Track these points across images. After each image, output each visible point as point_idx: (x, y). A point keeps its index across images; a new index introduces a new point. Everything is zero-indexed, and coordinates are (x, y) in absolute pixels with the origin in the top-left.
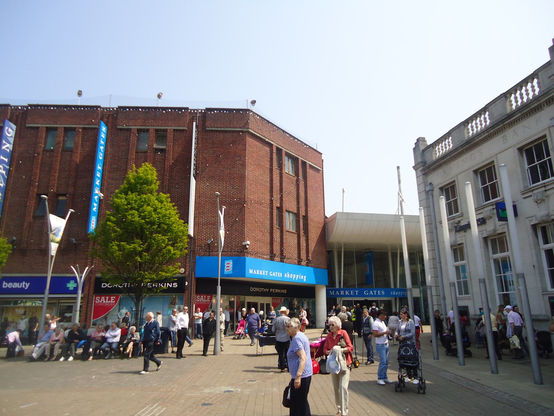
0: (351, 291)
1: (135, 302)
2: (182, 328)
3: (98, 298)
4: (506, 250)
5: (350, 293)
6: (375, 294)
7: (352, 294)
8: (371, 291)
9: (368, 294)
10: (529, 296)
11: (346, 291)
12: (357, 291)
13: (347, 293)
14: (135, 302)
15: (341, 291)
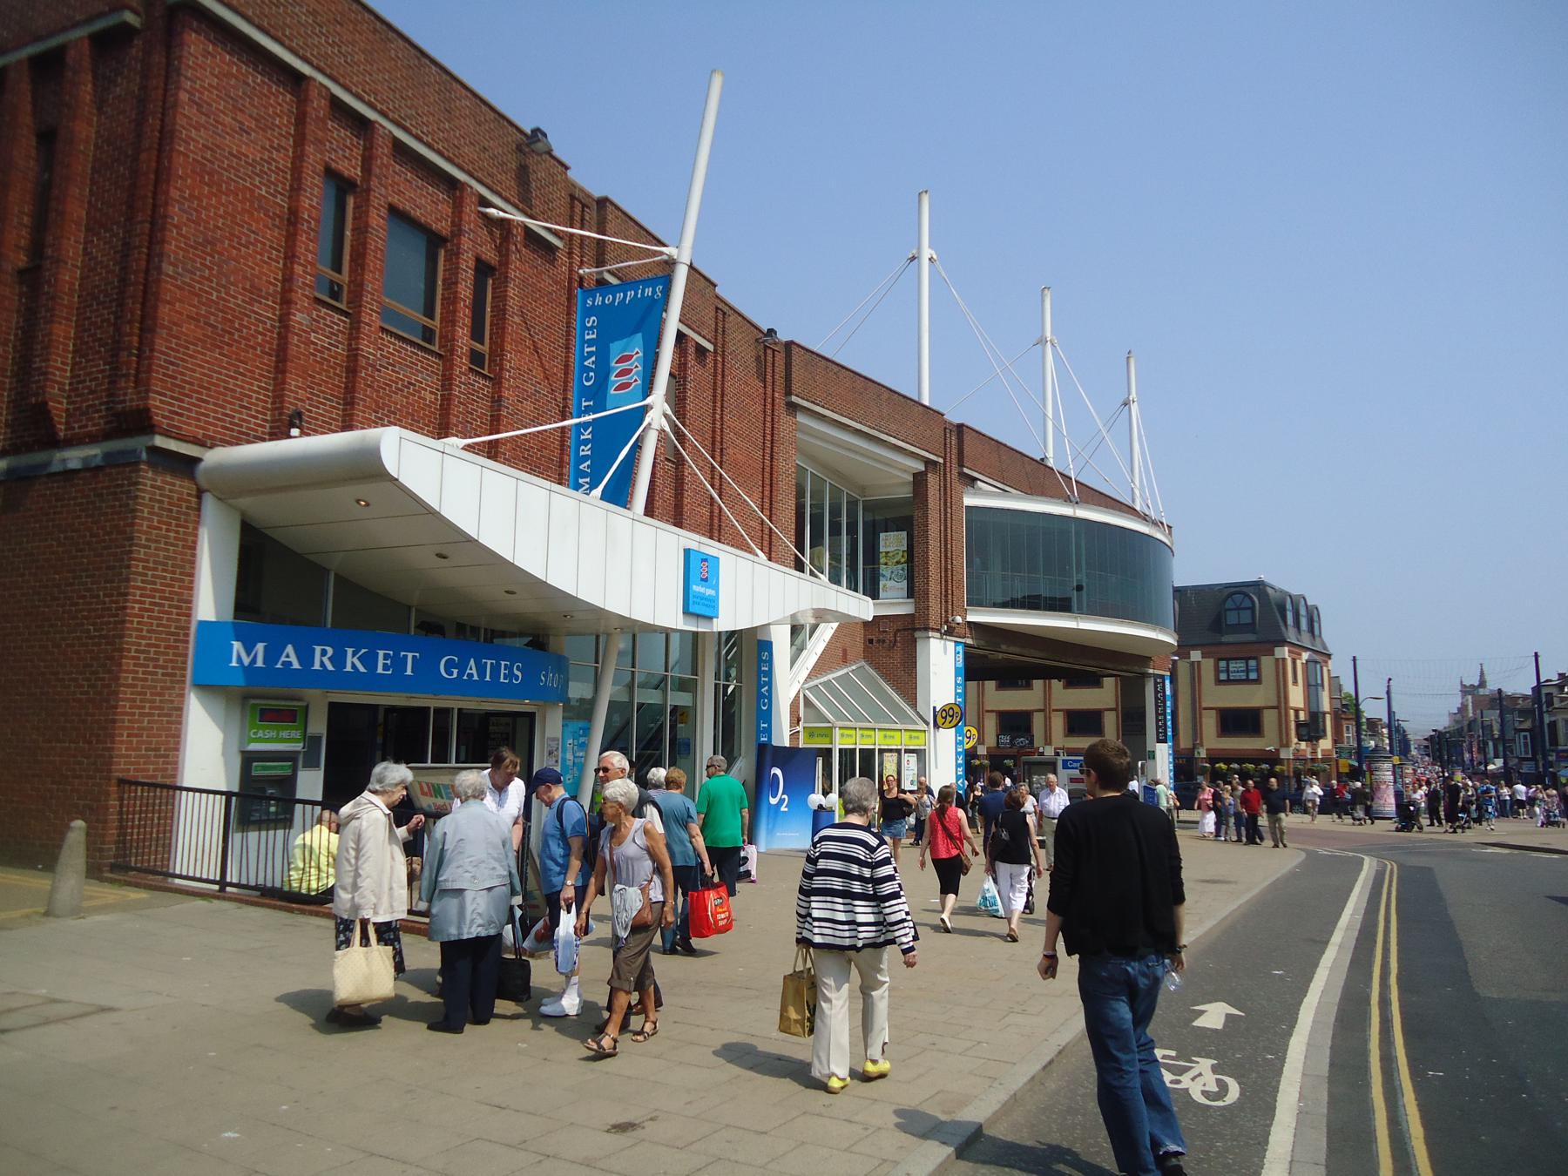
0: (381, 653)
1: (520, 1010)
2: (1070, 953)
3: (594, 321)
4: (566, 714)
5: (369, 660)
6: (594, 349)
7: (380, 670)
8: (472, 662)
9: (592, 374)
10: (594, 652)
11: (350, 651)
12: (410, 655)
13: (352, 661)
14: (520, 1010)
15: (318, 649)
